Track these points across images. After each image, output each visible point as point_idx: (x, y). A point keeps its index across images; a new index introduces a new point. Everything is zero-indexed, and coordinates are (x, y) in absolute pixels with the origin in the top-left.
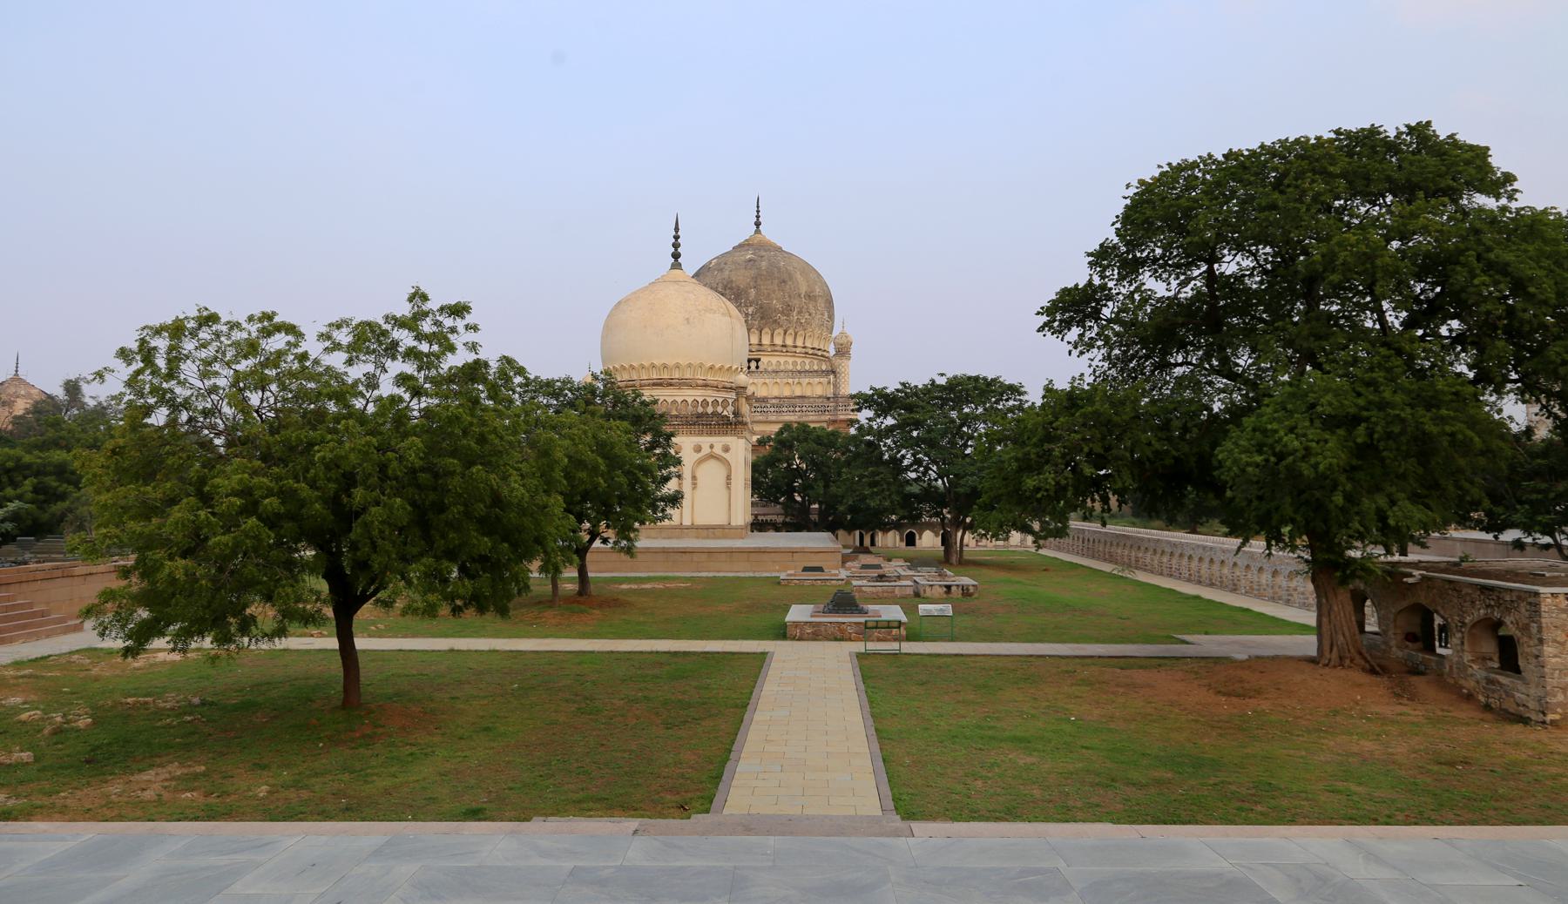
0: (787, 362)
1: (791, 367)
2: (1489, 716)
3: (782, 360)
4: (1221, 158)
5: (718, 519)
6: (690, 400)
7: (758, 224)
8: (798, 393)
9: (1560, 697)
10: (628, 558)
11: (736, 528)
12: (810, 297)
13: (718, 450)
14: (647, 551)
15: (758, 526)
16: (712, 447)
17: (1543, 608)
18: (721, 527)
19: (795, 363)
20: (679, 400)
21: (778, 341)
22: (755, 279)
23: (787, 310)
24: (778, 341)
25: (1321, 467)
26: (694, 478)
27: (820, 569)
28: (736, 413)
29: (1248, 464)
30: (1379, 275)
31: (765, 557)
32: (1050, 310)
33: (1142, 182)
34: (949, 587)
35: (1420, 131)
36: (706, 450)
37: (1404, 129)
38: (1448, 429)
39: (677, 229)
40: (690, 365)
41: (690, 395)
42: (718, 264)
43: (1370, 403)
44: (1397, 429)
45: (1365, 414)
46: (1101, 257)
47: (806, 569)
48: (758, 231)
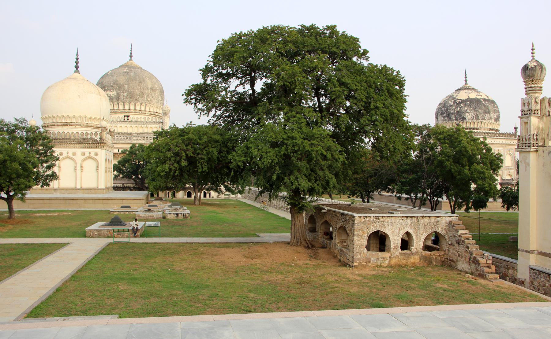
0: (141, 117)
1: (143, 120)
2: (339, 264)
3: (139, 116)
4: (255, 32)
5: (93, 185)
6: (80, 132)
7: (131, 57)
8: (146, 131)
9: (359, 256)
10: (21, 202)
11: (101, 189)
12: (152, 89)
13: (93, 155)
14: (383, 195)
15: (116, 189)
16: (90, 153)
17: (356, 222)
18: (94, 189)
19: (145, 118)
20: (75, 132)
21: (138, 108)
22: (128, 80)
23: (142, 94)
24: (138, 108)
25: (265, 163)
26: (82, 167)
27: (129, 207)
28: (101, 139)
29: (239, 161)
30: (297, 84)
31: (110, 202)
32: (189, 93)
33: (223, 40)
34: (177, 214)
35: (332, 28)
36: (87, 155)
37: (326, 28)
38: (315, 149)
39: (77, 55)
40: (80, 117)
41: (80, 130)
42: (112, 73)
43: (288, 137)
44: (296, 148)
45: (286, 141)
46: (206, 71)
47: (122, 207)
48: (131, 60)
